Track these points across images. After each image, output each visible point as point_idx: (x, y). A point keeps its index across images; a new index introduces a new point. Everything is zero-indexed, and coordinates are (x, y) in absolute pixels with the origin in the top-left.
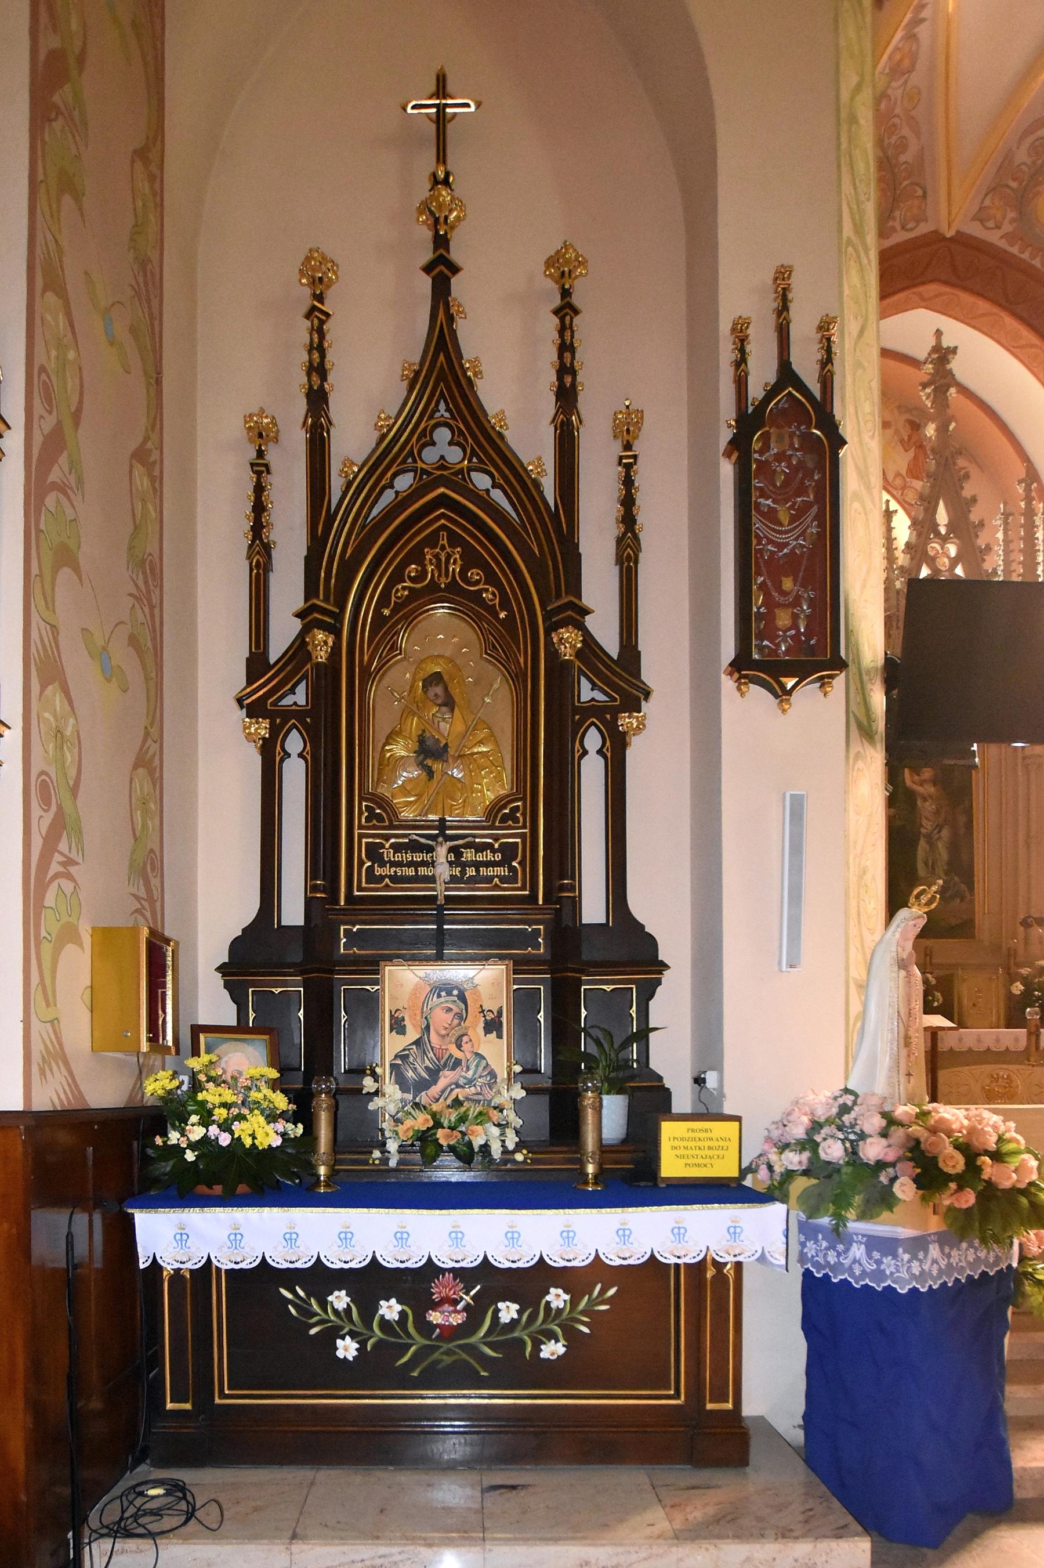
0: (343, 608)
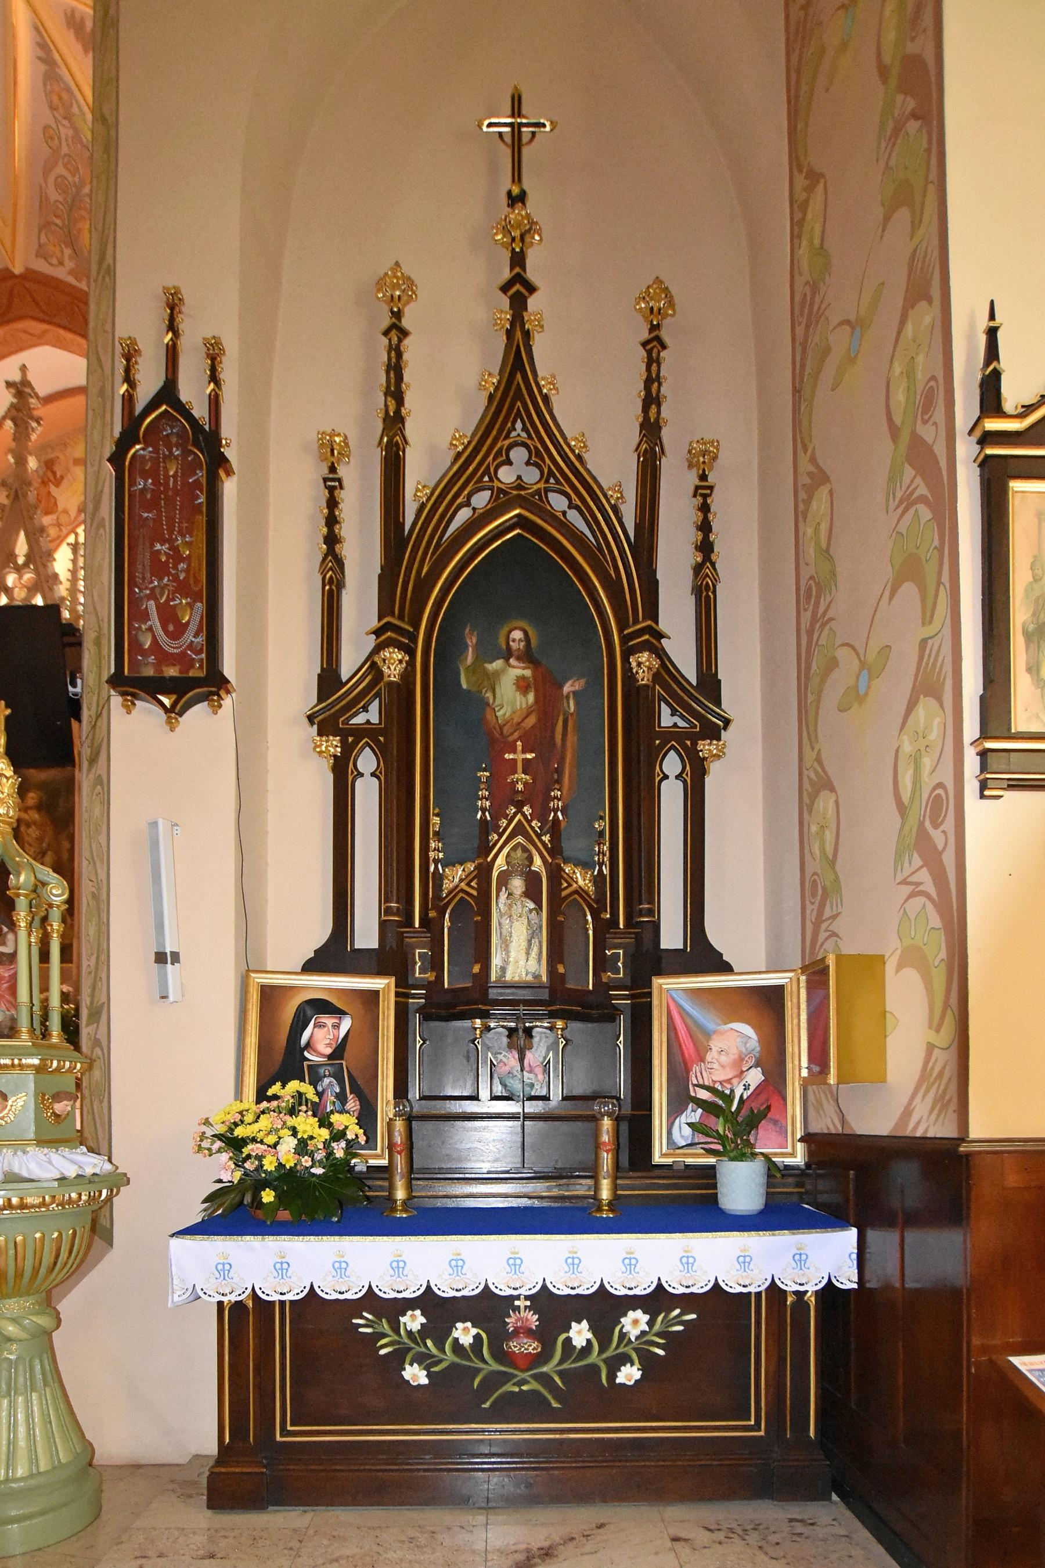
0: (417, 628)
